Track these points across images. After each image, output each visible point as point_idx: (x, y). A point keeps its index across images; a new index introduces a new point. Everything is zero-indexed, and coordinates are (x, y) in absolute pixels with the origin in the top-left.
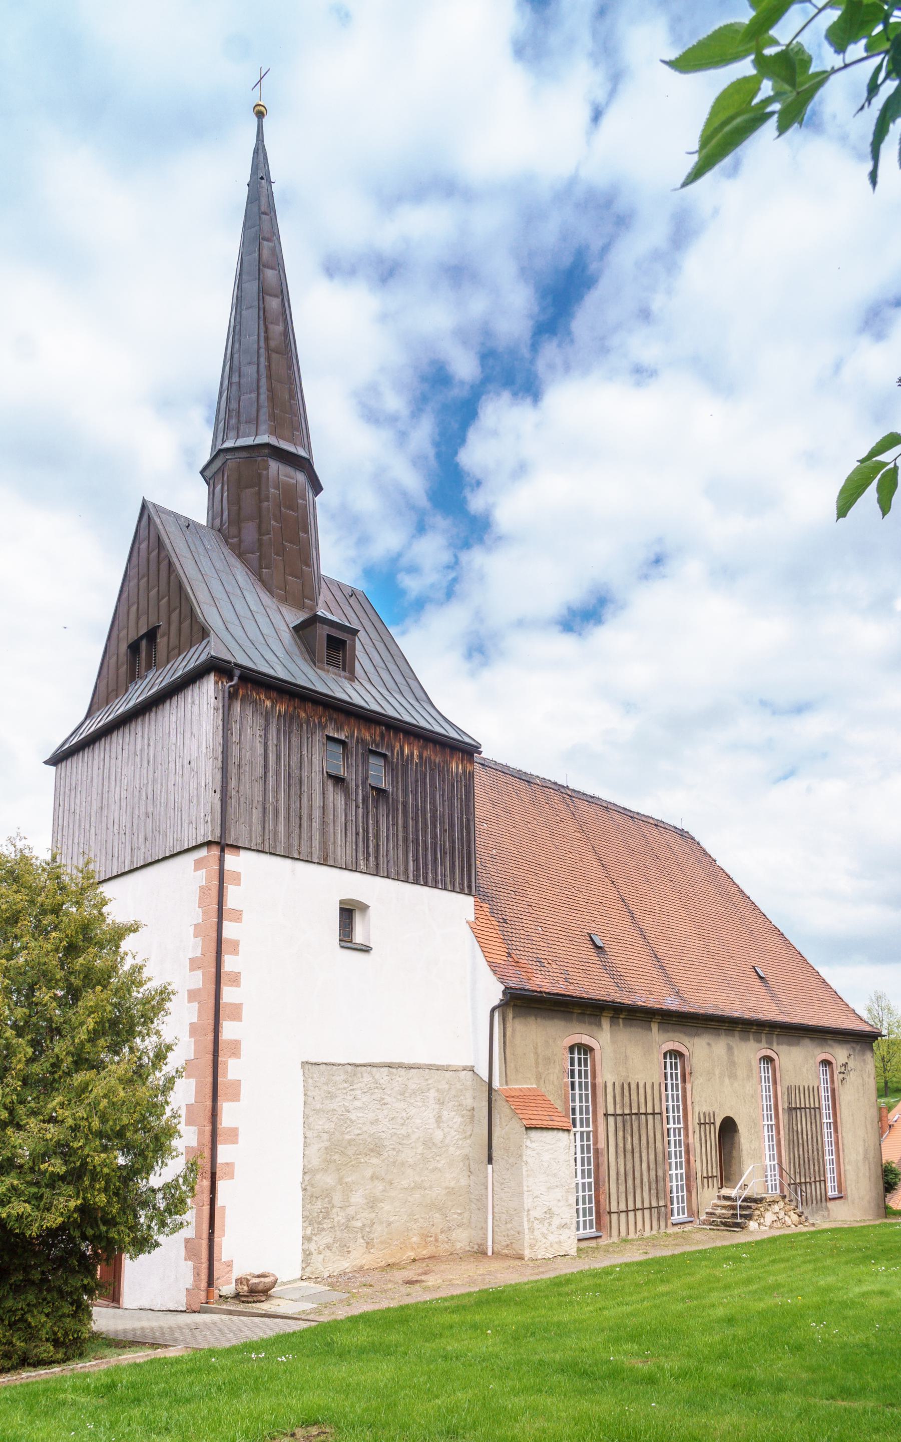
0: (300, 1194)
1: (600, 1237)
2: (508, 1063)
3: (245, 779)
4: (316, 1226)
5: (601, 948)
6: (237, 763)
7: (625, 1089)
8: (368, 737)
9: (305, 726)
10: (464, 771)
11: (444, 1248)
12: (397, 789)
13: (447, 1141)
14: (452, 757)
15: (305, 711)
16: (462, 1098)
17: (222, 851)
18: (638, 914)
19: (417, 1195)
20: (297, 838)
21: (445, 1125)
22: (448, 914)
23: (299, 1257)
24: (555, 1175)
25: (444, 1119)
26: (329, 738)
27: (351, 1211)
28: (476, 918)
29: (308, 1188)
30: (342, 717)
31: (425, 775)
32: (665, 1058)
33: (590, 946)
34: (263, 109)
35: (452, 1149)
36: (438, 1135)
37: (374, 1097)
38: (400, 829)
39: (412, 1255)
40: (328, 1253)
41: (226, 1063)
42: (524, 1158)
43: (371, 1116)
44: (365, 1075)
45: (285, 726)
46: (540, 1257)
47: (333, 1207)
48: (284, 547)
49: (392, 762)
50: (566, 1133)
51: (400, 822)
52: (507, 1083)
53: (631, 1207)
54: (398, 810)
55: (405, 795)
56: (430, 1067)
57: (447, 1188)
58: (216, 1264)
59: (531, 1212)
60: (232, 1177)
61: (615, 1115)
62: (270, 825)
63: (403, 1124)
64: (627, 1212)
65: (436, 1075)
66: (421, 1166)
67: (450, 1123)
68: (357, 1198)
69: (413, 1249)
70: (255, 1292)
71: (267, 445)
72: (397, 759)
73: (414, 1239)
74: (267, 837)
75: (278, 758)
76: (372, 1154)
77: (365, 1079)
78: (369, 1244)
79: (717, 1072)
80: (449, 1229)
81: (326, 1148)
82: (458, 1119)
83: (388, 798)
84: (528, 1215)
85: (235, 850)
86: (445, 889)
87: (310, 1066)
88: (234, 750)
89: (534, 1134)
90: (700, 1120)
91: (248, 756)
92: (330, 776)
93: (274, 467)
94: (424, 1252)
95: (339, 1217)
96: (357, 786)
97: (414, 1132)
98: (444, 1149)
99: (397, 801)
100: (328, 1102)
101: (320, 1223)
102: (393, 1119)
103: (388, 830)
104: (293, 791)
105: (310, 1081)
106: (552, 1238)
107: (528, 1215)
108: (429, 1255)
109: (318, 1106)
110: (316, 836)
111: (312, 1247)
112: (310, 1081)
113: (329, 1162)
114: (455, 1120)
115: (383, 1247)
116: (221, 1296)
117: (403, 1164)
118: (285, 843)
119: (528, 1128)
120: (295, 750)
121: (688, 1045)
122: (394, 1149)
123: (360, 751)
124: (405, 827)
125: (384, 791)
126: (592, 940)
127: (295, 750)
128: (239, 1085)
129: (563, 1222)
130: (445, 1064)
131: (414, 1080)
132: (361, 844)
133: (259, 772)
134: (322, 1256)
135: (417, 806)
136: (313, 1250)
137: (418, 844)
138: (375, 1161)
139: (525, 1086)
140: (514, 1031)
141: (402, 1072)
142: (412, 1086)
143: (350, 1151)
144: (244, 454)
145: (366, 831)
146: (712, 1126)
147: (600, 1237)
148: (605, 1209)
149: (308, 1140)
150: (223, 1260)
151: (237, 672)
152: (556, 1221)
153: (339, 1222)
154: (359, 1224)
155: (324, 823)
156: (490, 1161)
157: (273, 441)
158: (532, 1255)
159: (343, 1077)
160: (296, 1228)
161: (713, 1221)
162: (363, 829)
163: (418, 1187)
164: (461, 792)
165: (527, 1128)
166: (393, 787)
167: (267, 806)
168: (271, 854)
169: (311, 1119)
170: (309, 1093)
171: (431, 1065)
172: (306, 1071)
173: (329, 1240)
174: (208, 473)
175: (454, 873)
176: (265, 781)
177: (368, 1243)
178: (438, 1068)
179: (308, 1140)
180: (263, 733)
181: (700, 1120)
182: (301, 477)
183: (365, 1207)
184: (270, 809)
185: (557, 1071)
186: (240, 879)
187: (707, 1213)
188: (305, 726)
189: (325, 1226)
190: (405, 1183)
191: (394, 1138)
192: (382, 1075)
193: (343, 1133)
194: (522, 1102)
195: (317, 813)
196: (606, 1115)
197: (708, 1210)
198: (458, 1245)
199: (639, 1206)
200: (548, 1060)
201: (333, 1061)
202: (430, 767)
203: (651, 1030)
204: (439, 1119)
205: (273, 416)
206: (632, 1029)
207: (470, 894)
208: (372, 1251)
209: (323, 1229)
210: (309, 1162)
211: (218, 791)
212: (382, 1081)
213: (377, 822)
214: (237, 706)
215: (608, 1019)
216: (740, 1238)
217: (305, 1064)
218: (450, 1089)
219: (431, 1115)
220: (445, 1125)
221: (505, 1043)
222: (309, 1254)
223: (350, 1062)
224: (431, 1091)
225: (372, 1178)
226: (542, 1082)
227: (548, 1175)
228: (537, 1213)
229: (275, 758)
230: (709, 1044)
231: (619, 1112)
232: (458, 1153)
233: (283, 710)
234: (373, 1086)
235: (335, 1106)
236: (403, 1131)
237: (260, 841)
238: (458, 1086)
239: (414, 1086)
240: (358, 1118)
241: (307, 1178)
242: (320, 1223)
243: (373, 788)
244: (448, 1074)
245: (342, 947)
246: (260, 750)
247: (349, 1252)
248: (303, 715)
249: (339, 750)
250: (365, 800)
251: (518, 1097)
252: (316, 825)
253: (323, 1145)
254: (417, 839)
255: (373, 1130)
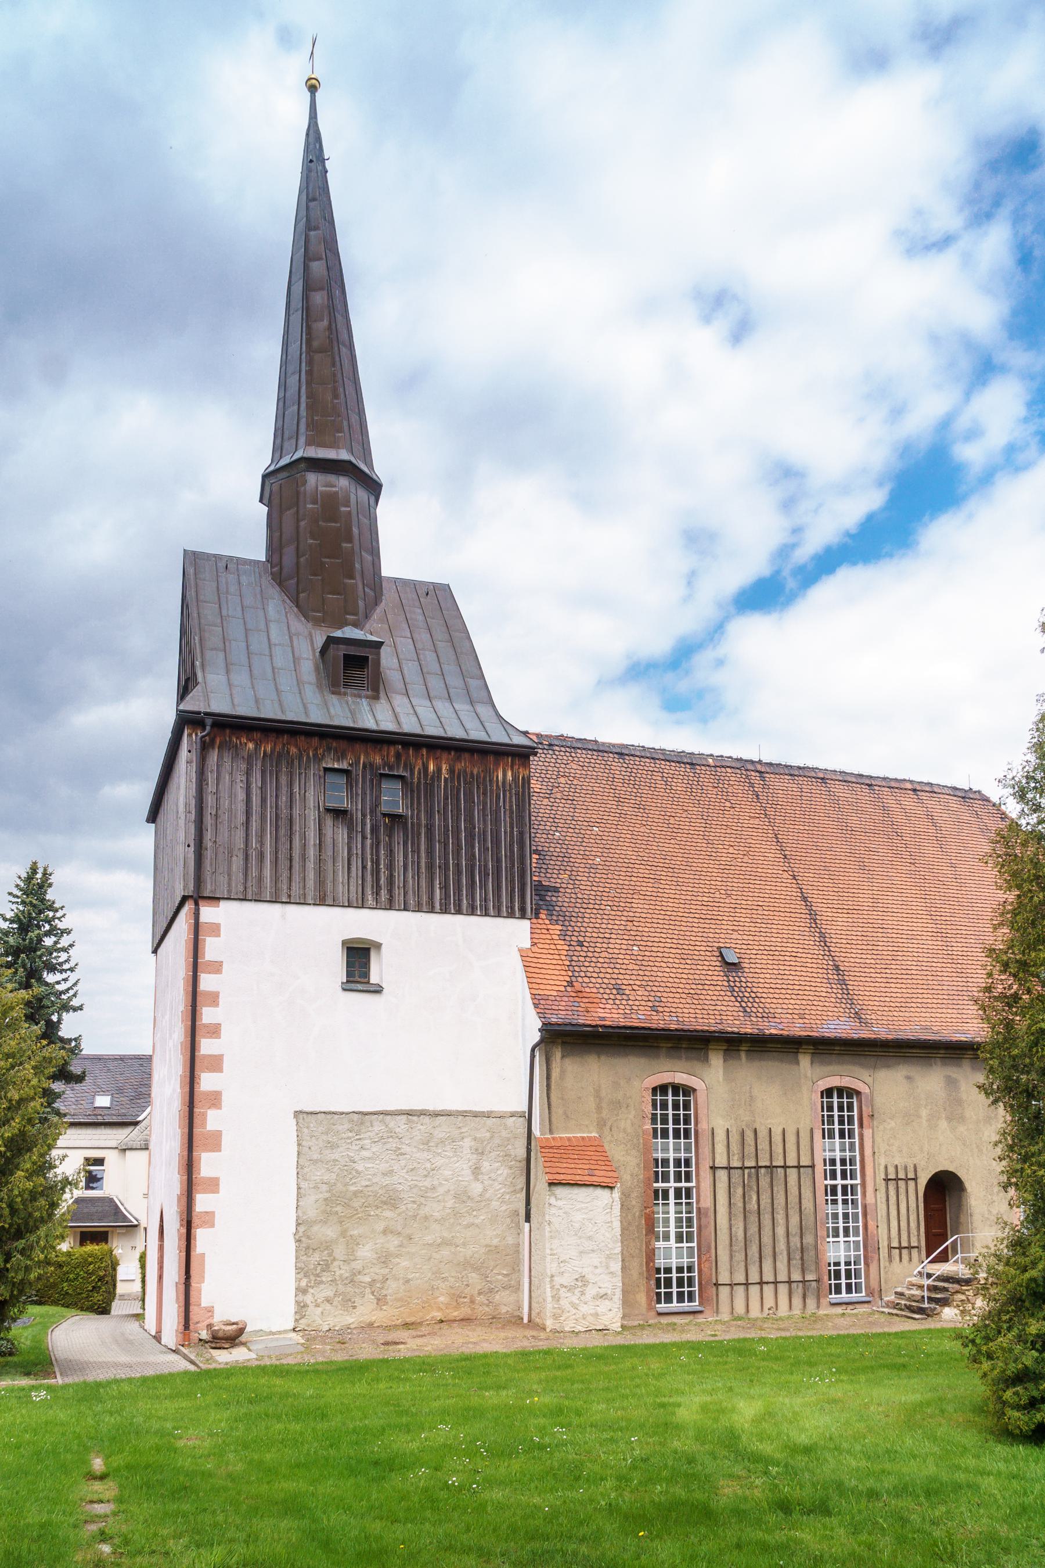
0: (293, 1246)
1: (701, 1312)
2: (553, 1109)
3: (224, 830)
4: (312, 1278)
5: (734, 964)
6: (214, 813)
7: (747, 1137)
8: (378, 760)
9: (296, 763)
10: (515, 778)
11: (482, 1310)
12: (419, 811)
13: (487, 1195)
14: (497, 765)
15: (296, 746)
16: (510, 1147)
17: (197, 904)
18: (825, 913)
19: (445, 1252)
20: (285, 881)
21: (486, 1177)
22: (499, 942)
23: (291, 1308)
24: (590, 1238)
25: (484, 1170)
26: (326, 770)
27: (357, 1265)
28: (534, 944)
29: (303, 1239)
30: (343, 744)
31: (459, 790)
32: (822, 1097)
33: (718, 964)
34: (314, 81)
35: (495, 1204)
36: (476, 1188)
37: (388, 1146)
38: (423, 855)
39: (439, 1315)
40: (328, 1307)
41: (204, 1115)
42: (547, 1218)
43: (384, 1167)
44: (375, 1123)
45: (272, 766)
46: (567, 1329)
47: (334, 1259)
48: (323, 564)
49: (412, 783)
50: (607, 1192)
51: (423, 847)
52: (551, 1131)
53: (754, 1277)
54: (419, 834)
55: (430, 816)
56: (464, 1114)
57: (486, 1246)
58: (193, 1309)
59: (555, 1278)
60: (213, 1226)
61: (729, 1168)
62: (254, 872)
63: (426, 1176)
64: (747, 1284)
65: (472, 1123)
66: (452, 1221)
67: (493, 1175)
68: (366, 1252)
69: (439, 1309)
70: (232, 1338)
71: (302, 459)
72: (419, 779)
73: (442, 1299)
74: (249, 884)
75: (263, 800)
76: (385, 1207)
77: (376, 1129)
78: (381, 1301)
79: (924, 1113)
80: (491, 1290)
81: (326, 1199)
82: (504, 1171)
83: (406, 823)
84: (552, 1281)
85: (214, 902)
86: (487, 915)
87: (305, 1115)
88: (210, 800)
89: (559, 1191)
90: (886, 1174)
91: (225, 803)
92: (328, 810)
93: (313, 479)
94: (456, 1314)
95: (342, 1271)
96: (364, 815)
97: (441, 1184)
98: (483, 1204)
99: (419, 825)
100: (328, 1151)
101: (318, 1275)
102: (412, 1170)
103: (405, 857)
104: (282, 832)
105: (305, 1130)
106: (584, 1309)
107: (552, 1281)
108: (461, 1317)
109: (315, 1157)
110: (311, 875)
111: (308, 1299)
112: (305, 1130)
113: (330, 1213)
114: (499, 1172)
115: (399, 1304)
116: (201, 1340)
117: (426, 1218)
118: (271, 888)
119: (551, 1184)
120: (284, 790)
121: (869, 1080)
122: (414, 1202)
123: (368, 777)
124: (430, 852)
125: (400, 816)
126: (721, 955)
127: (284, 790)
128: (221, 1135)
129: (602, 1291)
130: (485, 1110)
131: (443, 1128)
132: (369, 878)
133: (241, 818)
134: (320, 1310)
135: (446, 827)
136: (308, 1302)
137: (447, 868)
138: (388, 1214)
139: (579, 1135)
140: (563, 1072)
141: (426, 1119)
142: (439, 1134)
143: (356, 1203)
144: (284, 474)
145: (376, 863)
146: (912, 1184)
147: (701, 1312)
148: (711, 1279)
149: (302, 1191)
150: (203, 1305)
151: (209, 721)
152: (591, 1291)
153: (341, 1276)
154: (367, 1279)
155: (320, 861)
156: (528, 1219)
157: (313, 452)
158: (557, 1327)
159: (347, 1126)
160: (288, 1280)
161: (898, 1304)
162: (372, 861)
163: (446, 1243)
164: (511, 802)
165: (551, 1184)
166: (412, 810)
167: (250, 852)
168: (256, 900)
169: (306, 1170)
170: (304, 1143)
171: (466, 1112)
172: (301, 1121)
173: (330, 1293)
174: (266, 501)
175: (499, 897)
176: (247, 828)
177: (379, 1300)
178: (476, 1115)
179: (302, 1191)
180: (244, 778)
181: (886, 1174)
182: (343, 482)
183: (375, 1261)
184: (253, 854)
185: (631, 1116)
186: (219, 930)
187: (896, 1293)
188: (296, 763)
189: (324, 1279)
190: (429, 1239)
191: (415, 1190)
192: (400, 1124)
193: (346, 1184)
194: (557, 1151)
195: (312, 852)
196: (713, 1168)
197: (899, 1290)
198: (504, 1309)
199: (768, 1276)
200: (617, 1105)
201: (333, 1110)
202: (465, 780)
203: (798, 1063)
204: (476, 1171)
205: (311, 425)
206: (764, 1063)
207: (523, 916)
208: (384, 1308)
209: (322, 1282)
210: (304, 1213)
211: (192, 845)
212: (397, 1130)
213: (391, 853)
214: (213, 756)
215: (722, 1053)
216: (931, 1324)
217: (297, 1114)
218: (491, 1137)
219: (465, 1166)
220: (486, 1177)
221: (548, 1086)
222: (304, 1306)
223: (356, 1110)
224: (466, 1140)
225: (385, 1232)
226: (606, 1130)
227: (580, 1238)
228: (567, 1280)
229: (259, 802)
230: (908, 1078)
231: (736, 1163)
232: (504, 1208)
233: (269, 749)
234: (385, 1135)
235: (336, 1156)
236: (427, 1183)
237: (241, 888)
238: (504, 1134)
239: (441, 1135)
240: (367, 1169)
241: (302, 1229)
242: (318, 1275)
243: (385, 815)
244: (490, 1122)
245: (344, 990)
246: (241, 795)
247: (354, 1307)
248: (293, 750)
249: (342, 780)
250: (375, 830)
251: (558, 1148)
252: (311, 865)
253: (321, 1196)
254: (447, 864)
255: (386, 1181)
